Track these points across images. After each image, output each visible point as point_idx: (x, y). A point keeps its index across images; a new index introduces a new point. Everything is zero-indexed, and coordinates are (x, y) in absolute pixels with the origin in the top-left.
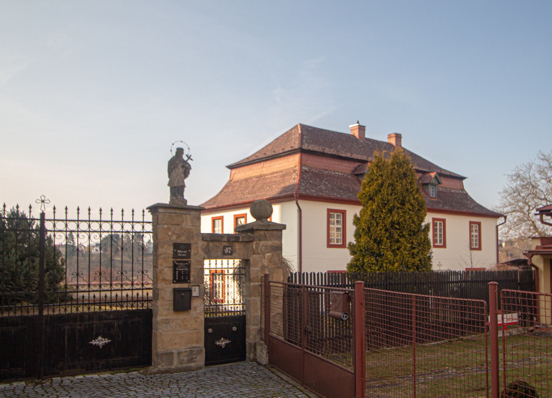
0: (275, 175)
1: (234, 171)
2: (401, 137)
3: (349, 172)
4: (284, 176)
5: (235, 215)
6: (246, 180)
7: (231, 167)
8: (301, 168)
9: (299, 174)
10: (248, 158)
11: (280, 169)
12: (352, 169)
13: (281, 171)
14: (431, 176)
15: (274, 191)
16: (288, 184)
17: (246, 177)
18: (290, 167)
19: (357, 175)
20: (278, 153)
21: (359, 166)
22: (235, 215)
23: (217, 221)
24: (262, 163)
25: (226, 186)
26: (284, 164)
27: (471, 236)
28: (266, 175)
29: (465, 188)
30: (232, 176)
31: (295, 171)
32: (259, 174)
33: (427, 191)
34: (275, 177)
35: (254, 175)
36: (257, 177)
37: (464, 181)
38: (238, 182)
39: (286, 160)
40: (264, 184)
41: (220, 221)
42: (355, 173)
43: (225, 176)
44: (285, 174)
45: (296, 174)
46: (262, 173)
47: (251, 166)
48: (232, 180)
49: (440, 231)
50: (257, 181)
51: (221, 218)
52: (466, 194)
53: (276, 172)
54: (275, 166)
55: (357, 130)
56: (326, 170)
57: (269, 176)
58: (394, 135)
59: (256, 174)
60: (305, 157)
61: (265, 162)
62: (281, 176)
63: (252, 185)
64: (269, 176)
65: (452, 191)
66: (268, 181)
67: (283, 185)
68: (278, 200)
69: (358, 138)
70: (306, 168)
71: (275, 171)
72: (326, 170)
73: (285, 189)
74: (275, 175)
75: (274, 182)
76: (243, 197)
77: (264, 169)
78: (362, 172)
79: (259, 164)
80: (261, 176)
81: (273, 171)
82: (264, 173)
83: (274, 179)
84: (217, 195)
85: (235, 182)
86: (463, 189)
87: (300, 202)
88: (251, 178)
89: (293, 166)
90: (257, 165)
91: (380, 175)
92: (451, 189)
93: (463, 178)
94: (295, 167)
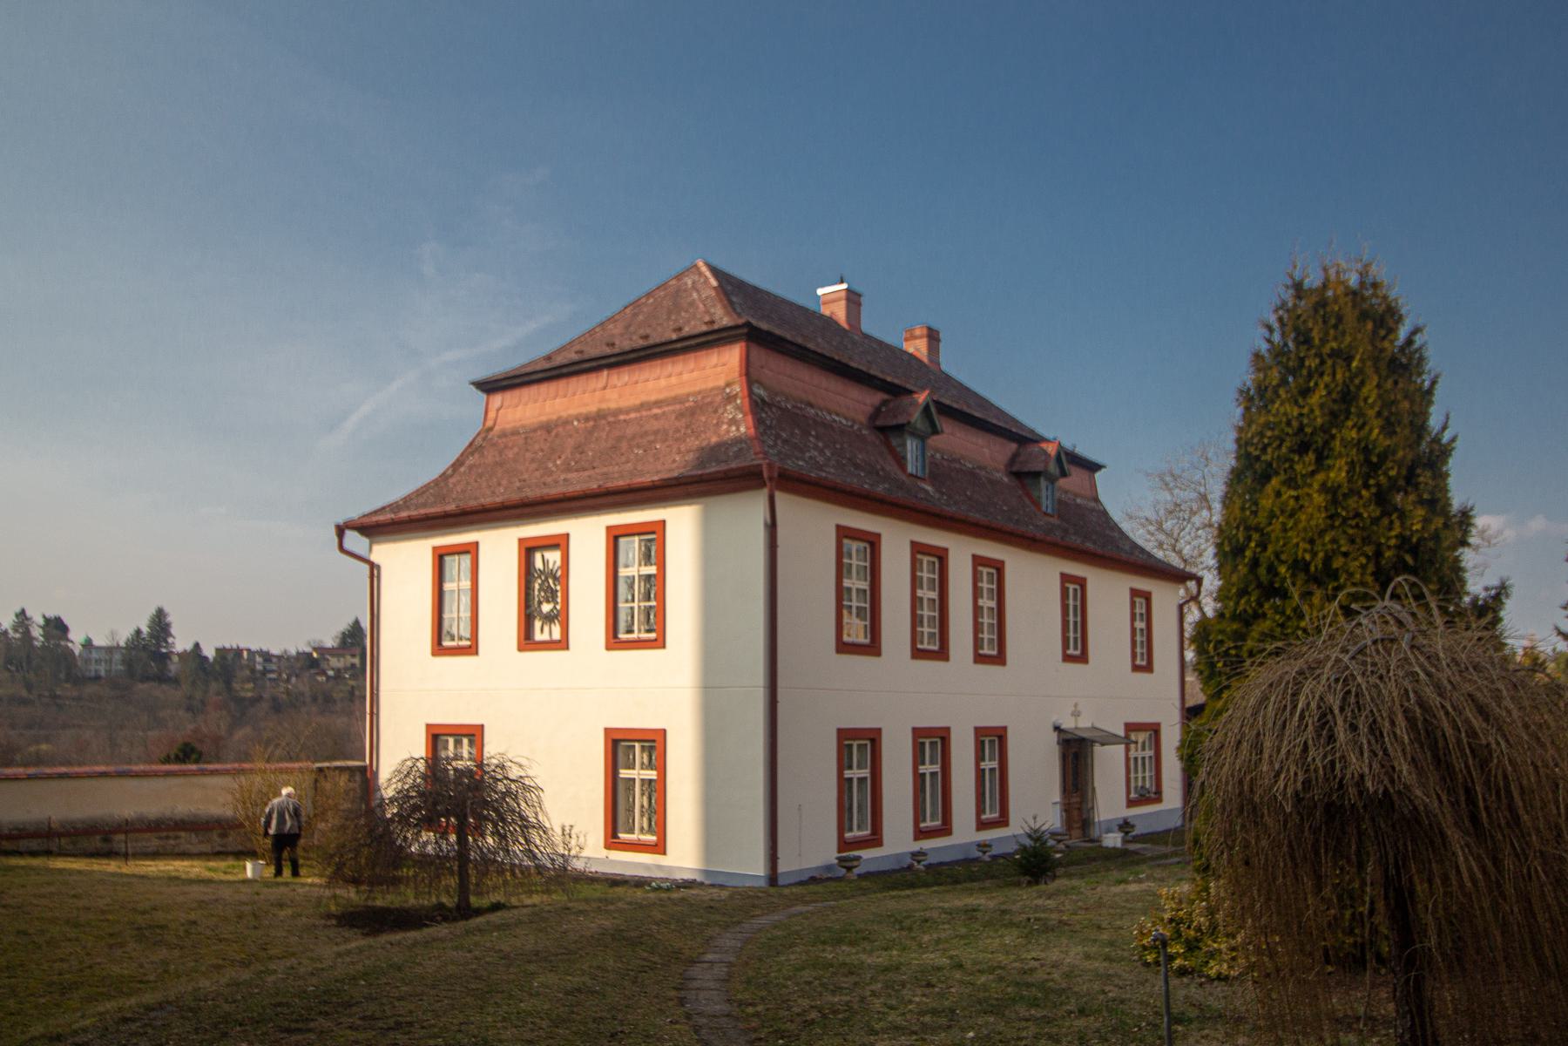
0: (656, 411)
1: (497, 399)
2: (938, 340)
3: (863, 419)
4: (692, 412)
5: (521, 541)
6: (547, 427)
7: (489, 387)
8: (751, 393)
9: (747, 407)
10: (549, 358)
11: (673, 394)
12: (869, 410)
13: (676, 400)
14: (1045, 452)
15: (674, 461)
16: (714, 440)
17: (544, 418)
18: (711, 385)
19: (882, 430)
20: (658, 340)
21: (884, 403)
22: (521, 541)
23: (451, 562)
24: (605, 373)
25: (472, 448)
26: (686, 377)
27: (1133, 630)
28: (619, 411)
29: (1102, 498)
30: (492, 415)
31: (730, 399)
32: (593, 408)
33: (1035, 494)
34: (656, 417)
35: (573, 412)
36: (587, 418)
37: (1097, 475)
38: (515, 433)
39: (692, 365)
40: (619, 439)
41: (466, 560)
42: (879, 423)
43: (469, 414)
44: (695, 409)
45: (738, 408)
46: (604, 406)
47: (562, 383)
48: (491, 429)
49: (1075, 615)
50: (590, 432)
51: (472, 550)
52: (1105, 513)
53: (658, 403)
54: (650, 385)
55: (843, 303)
56: (811, 406)
57: (633, 415)
58: (925, 332)
59: (584, 410)
60: (759, 354)
61: (614, 371)
62: (680, 415)
63: (571, 442)
64: (633, 415)
65: (1078, 501)
66: (630, 431)
67: (694, 443)
68: (691, 489)
69: (845, 326)
70: (762, 392)
71: (653, 398)
72: (811, 406)
73: (713, 453)
74: (656, 411)
75: (656, 433)
76: (549, 480)
77: (609, 393)
78: (901, 420)
79: (593, 376)
80: (600, 416)
81: (644, 398)
82: (613, 405)
83: (656, 425)
84: (444, 477)
85: (503, 434)
86: (1096, 500)
87: (780, 497)
88: (566, 422)
89: (722, 383)
90: (583, 378)
91: (1334, 354)
92: (1076, 495)
93: (1093, 467)
94: (728, 385)
